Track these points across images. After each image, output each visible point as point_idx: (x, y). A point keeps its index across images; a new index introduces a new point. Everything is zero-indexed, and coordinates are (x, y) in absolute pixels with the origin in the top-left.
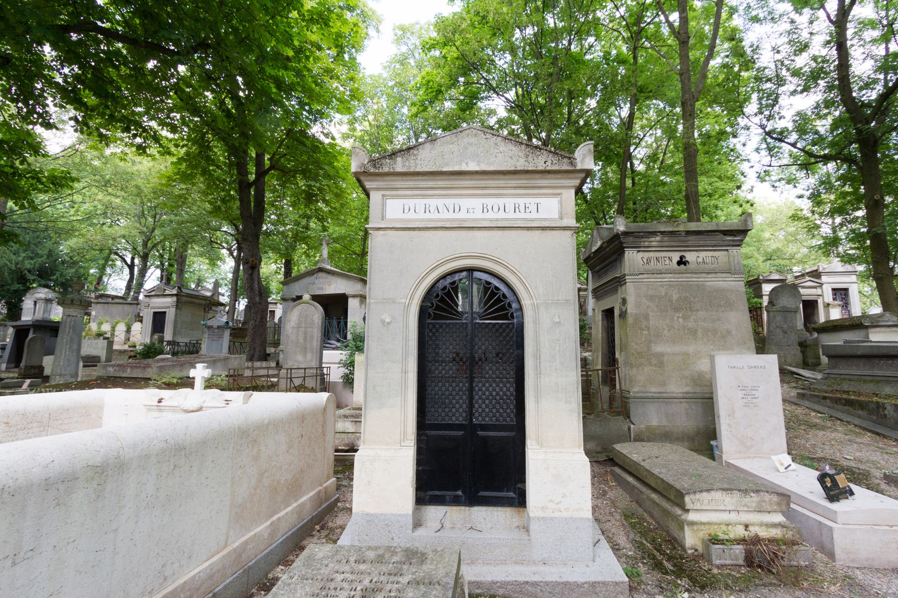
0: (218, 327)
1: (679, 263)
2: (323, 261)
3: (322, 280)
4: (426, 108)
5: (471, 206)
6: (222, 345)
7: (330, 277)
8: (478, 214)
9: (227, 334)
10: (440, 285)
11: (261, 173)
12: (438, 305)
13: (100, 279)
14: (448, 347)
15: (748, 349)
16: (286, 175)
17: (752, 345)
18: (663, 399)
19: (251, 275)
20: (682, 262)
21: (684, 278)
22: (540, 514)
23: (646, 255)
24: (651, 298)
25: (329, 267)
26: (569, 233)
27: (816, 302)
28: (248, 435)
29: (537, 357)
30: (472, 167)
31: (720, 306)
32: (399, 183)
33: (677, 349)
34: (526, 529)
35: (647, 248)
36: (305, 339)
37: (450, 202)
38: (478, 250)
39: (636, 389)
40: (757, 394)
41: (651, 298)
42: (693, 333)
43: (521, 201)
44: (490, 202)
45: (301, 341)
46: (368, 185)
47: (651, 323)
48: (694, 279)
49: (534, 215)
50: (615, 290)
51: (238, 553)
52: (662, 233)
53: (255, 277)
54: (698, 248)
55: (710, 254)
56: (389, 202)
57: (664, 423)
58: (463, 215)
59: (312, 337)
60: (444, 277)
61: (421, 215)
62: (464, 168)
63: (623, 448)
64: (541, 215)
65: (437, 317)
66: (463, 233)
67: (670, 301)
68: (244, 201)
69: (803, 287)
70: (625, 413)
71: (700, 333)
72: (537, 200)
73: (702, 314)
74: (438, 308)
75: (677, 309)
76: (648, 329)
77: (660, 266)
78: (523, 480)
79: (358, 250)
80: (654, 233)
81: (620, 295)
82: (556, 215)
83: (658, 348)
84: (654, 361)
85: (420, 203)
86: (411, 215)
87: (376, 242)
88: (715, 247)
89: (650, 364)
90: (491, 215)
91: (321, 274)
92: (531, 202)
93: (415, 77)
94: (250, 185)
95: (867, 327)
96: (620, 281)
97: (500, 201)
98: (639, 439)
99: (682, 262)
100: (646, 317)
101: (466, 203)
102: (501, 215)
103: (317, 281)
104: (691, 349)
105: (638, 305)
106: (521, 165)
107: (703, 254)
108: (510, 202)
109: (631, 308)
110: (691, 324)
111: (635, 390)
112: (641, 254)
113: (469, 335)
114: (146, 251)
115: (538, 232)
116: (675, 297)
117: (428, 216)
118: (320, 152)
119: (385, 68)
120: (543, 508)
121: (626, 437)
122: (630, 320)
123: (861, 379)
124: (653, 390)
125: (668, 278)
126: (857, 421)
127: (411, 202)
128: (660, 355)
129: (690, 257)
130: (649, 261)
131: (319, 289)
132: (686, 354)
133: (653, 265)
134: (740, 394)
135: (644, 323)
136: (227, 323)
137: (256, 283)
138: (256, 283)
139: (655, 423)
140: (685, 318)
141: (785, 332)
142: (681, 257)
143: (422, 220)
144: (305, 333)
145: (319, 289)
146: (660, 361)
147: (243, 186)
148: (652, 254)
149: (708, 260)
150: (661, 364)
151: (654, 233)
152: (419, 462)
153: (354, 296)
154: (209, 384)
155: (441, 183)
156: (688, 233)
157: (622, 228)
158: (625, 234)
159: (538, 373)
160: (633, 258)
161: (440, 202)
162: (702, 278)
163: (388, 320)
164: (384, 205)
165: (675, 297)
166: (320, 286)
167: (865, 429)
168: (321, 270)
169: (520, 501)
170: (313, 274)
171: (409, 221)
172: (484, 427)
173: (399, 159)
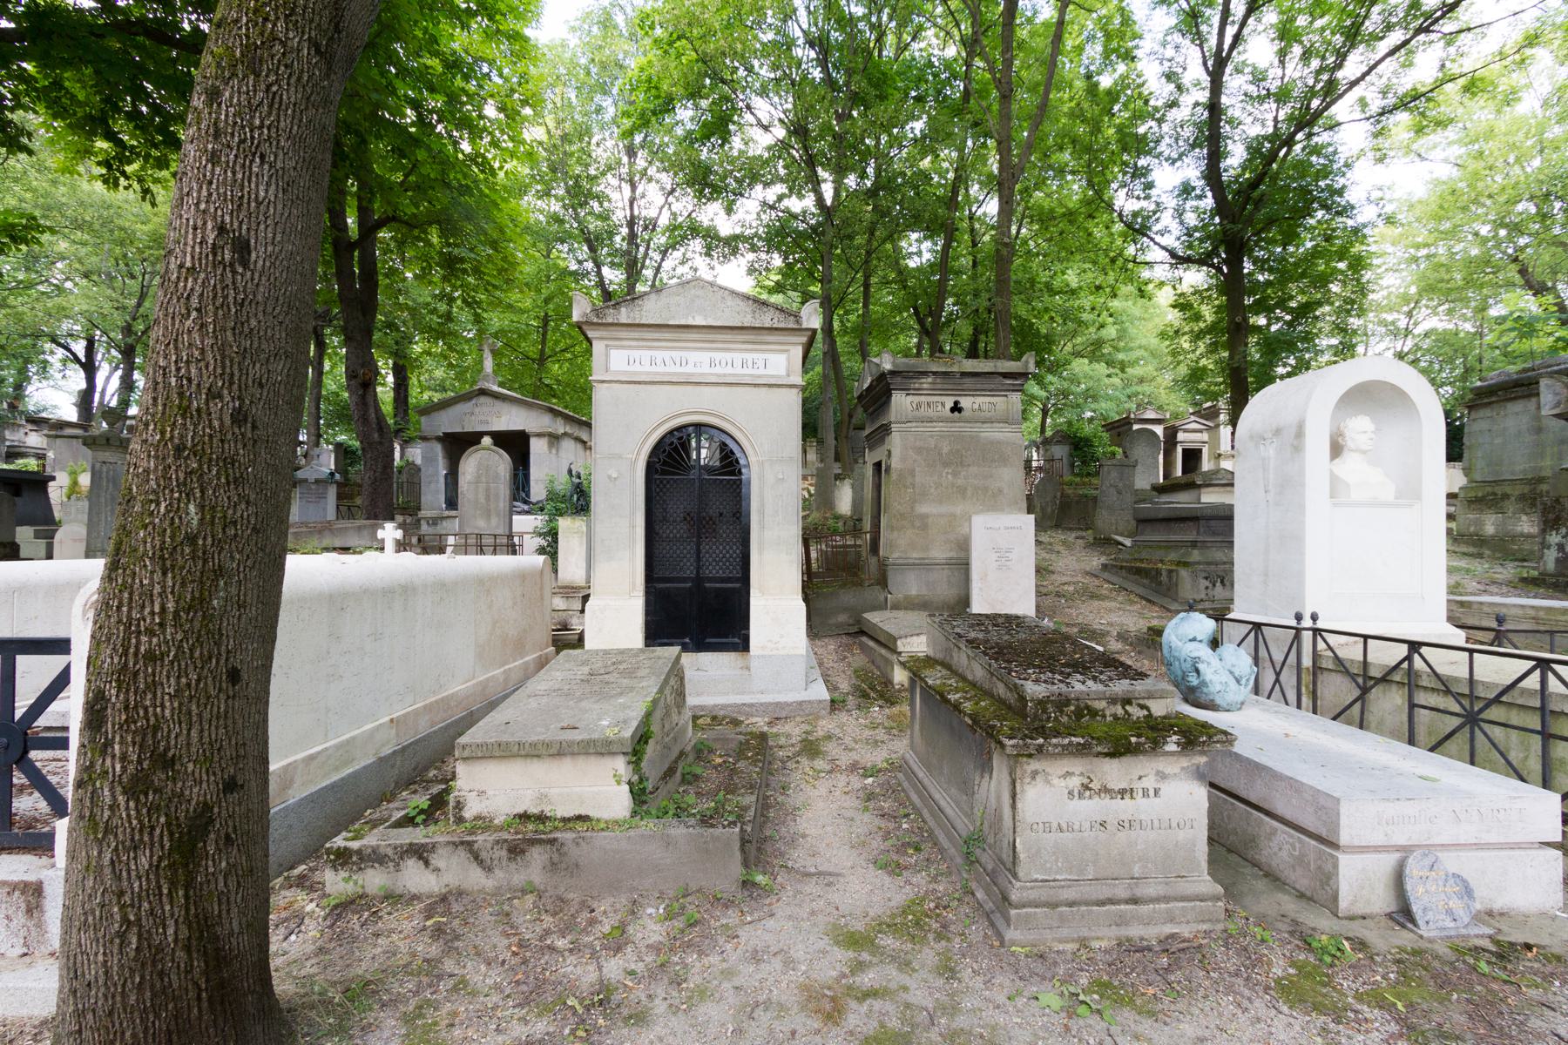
0: (317, 481)
1: (953, 410)
2: (486, 378)
3: (485, 409)
4: (648, 122)
5: (699, 360)
6: (325, 509)
7: (499, 404)
8: (706, 369)
9: (332, 492)
10: (668, 441)
11: (369, 229)
12: (669, 457)
13: (19, 387)
14: (678, 506)
15: (1020, 510)
16: (411, 228)
17: (1025, 505)
18: (924, 565)
19: (363, 397)
20: (956, 408)
21: (956, 428)
22: (760, 652)
23: (916, 399)
24: (919, 450)
25: (495, 388)
26: (795, 391)
27: (1200, 451)
28: (485, 584)
29: (762, 512)
30: (699, 321)
31: (993, 461)
32: (623, 334)
33: (944, 509)
34: (748, 668)
35: (918, 392)
36: (488, 498)
37: (676, 354)
38: (705, 407)
39: (896, 555)
40: (1011, 556)
41: (919, 450)
42: (962, 491)
43: (749, 356)
44: (718, 356)
45: (482, 500)
46: (590, 334)
47: (917, 479)
48: (967, 429)
49: (762, 371)
50: (882, 441)
51: (484, 685)
52: (934, 373)
53: (370, 400)
54: (974, 392)
55: (987, 399)
56: (613, 353)
57: (924, 592)
58: (689, 369)
59: (497, 495)
60: (671, 432)
61: (647, 368)
62: (691, 322)
63: (874, 617)
64: (769, 371)
65: (664, 472)
66: (690, 388)
67: (940, 454)
68: (343, 274)
69: (1186, 431)
70: (883, 582)
71: (969, 493)
72: (766, 356)
73: (974, 469)
74: (665, 463)
75: (946, 464)
76: (913, 486)
77: (930, 413)
78: (748, 628)
79: (533, 351)
80: (925, 374)
81: (886, 447)
82: (784, 373)
83: (923, 509)
84: (917, 524)
85: (646, 355)
86: (637, 368)
87: (601, 395)
88: (993, 392)
89: (913, 526)
90: (718, 370)
91: (483, 399)
92: (759, 357)
93: (636, 59)
94: (352, 246)
95: (1200, 486)
96: (885, 430)
97: (728, 356)
98: (896, 607)
99: (956, 408)
100: (912, 473)
101: (694, 356)
102: (729, 370)
103: (477, 410)
104: (958, 509)
105: (903, 459)
106: (748, 321)
107: (980, 400)
108: (738, 357)
109: (895, 463)
110: (960, 482)
111: (894, 556)
112: (910, 398)
113: (693, 490)
114: (130, 340)
115: (764, 390)
116: (945, 450)
117: (654, 369)
118: (472, 195)
119: (573, 29)
120: (763, 648)
121: (882, 606)
122: (894, 476)
123: (1159, 545)
124: (915, 555)
125: (939, 427)
126: (1140, 590)
127: (636, 354)
128: (924, 517)
129: (965, 402)
130: (919, 406)
131: (481, 422)
132: (954, 516)
133: (923, 411)
134: (994, 556)
135: (909, 480)
136: (332, 474)
137: (372, 410)
138: (372, 410)
139: (914, 592)
140: (955, 474)
141: (1119, 493)
142: (956, 403)
143: (648, 373)
144: (488, 490)
145: (481, 422)
146: (923, 523)
147: (342, 247)
148: (923, 398)
149: (984, 407)
150: (924, 527)
151: (925, 374)
152: (648, 613)
153: (539, 435)
154: (401, 546)
155: (667, 335)
156: (964, 374)
157: (888, 366)
158: (892, 373)
159: (762, 527)
160: (901, 402)
161: (666, 354)
162: (976, 428)
163: (615, 475)
164: (607, 356)
165: (945, 450)
166: (482, 418)
167: (1142, 598)
168: (483, 392)
169: (744, 646)
170: (470, 399)
171: (635, 373)
172: (711, 580)
173: (623, 310)
